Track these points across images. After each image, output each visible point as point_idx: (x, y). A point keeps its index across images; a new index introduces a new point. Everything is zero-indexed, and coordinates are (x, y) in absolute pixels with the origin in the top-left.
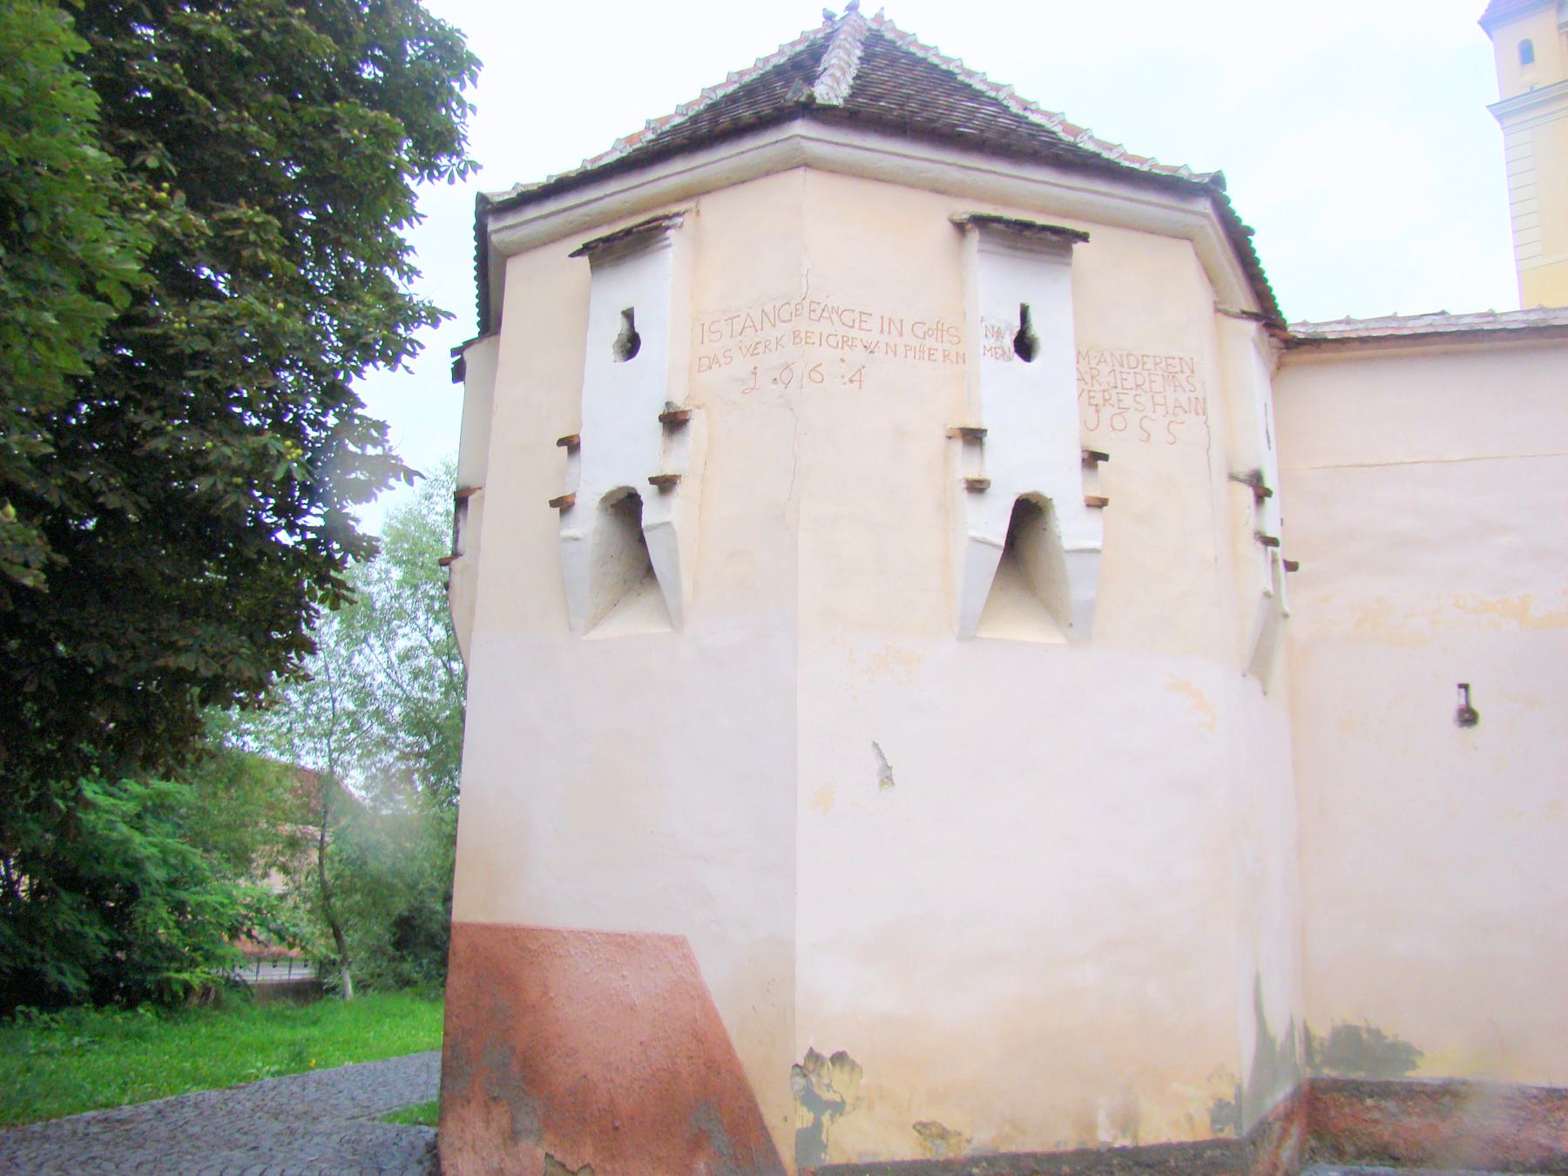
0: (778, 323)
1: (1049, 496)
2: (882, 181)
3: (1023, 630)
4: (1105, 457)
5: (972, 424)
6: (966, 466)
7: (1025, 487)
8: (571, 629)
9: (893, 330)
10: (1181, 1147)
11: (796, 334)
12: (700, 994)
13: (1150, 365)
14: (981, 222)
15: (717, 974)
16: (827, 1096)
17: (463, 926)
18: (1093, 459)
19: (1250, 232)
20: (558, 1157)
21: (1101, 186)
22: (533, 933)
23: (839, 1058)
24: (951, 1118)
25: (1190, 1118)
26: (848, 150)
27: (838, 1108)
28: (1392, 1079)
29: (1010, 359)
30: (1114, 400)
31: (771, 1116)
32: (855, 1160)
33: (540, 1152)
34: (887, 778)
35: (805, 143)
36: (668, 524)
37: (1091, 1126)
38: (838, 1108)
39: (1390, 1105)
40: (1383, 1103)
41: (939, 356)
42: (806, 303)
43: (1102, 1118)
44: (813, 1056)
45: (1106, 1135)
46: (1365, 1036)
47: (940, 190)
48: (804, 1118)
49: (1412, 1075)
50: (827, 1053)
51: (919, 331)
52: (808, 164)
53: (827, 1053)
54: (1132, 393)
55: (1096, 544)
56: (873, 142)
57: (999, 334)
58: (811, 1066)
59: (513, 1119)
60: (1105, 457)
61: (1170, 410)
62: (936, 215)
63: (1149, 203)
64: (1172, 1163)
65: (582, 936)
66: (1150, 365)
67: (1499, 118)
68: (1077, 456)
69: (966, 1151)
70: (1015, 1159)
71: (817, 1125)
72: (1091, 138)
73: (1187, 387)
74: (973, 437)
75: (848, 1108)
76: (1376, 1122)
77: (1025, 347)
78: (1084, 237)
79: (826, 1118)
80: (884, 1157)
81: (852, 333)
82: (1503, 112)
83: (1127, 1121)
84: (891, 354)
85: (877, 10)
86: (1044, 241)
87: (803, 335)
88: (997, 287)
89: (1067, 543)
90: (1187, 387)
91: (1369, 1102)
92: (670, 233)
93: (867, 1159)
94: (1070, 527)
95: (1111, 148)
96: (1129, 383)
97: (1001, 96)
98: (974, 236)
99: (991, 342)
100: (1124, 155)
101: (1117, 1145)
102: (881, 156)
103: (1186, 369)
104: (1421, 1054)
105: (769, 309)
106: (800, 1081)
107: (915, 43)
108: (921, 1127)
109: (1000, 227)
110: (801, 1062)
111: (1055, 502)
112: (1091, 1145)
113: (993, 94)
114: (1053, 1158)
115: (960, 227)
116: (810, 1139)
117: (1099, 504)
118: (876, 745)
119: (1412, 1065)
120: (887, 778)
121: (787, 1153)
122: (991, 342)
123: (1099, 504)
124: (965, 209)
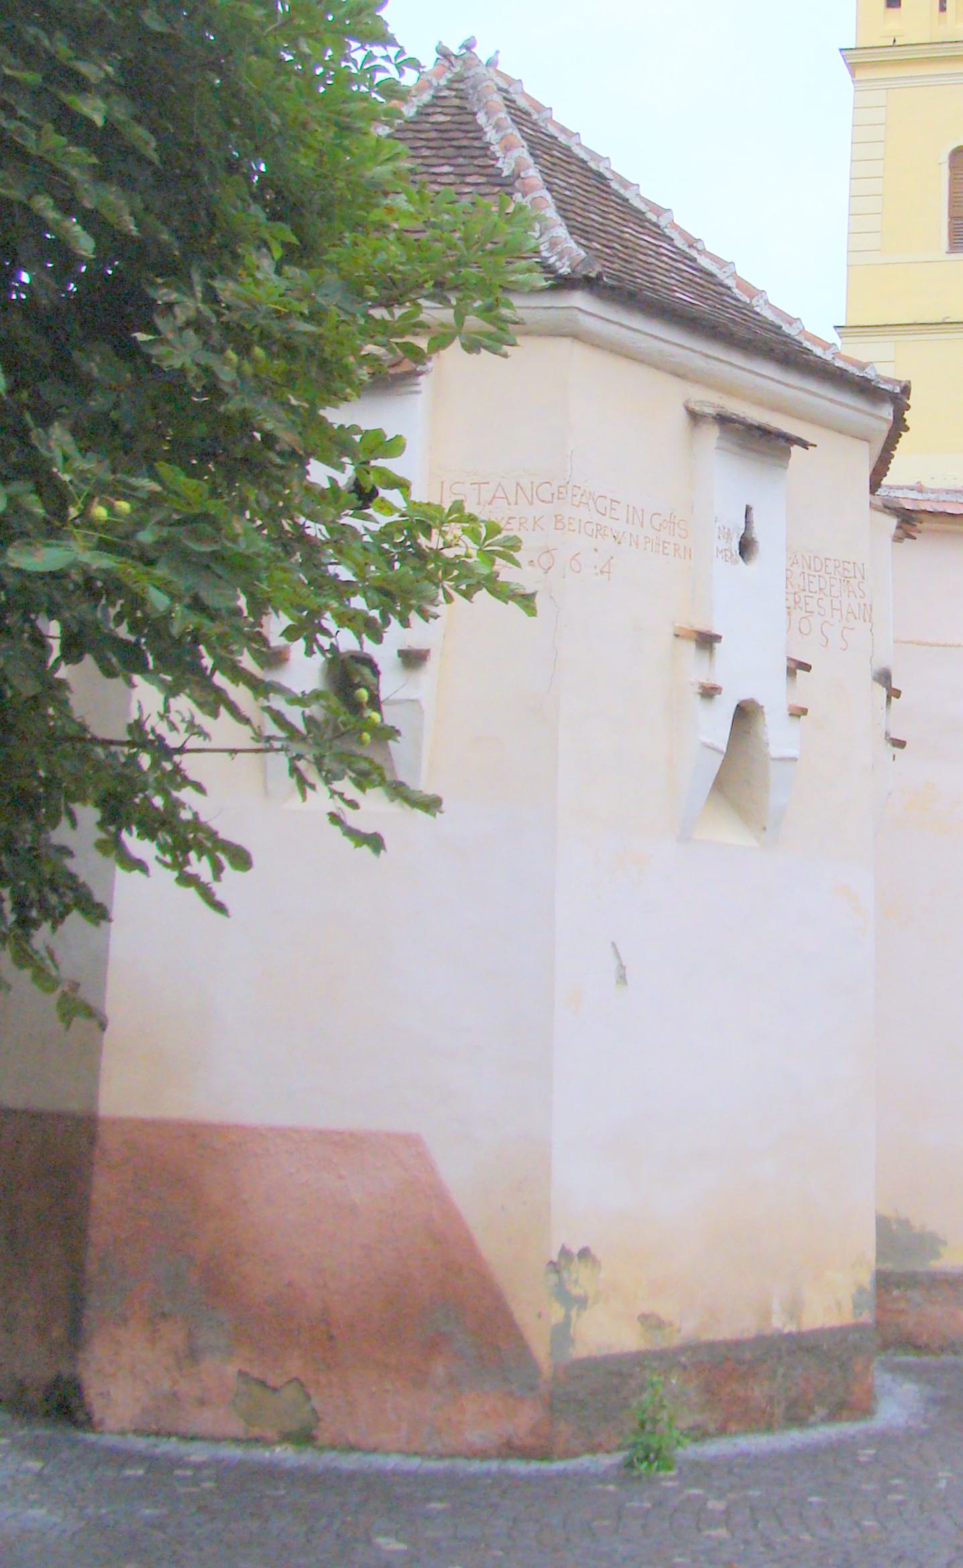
0: (536, 501)
1: (761, 703)
2: (642, 361)
3: (727, 833)
4: (807, 667)
5: (701, 626)
6: (696, 669)
7: (744, 695)
8: (267, 792)
9: (636, 521)
10: (832, 1331)
11: (558, 519)
12: (438, 1194)
13: (831, 569)
14: (724, 420)
15: (460, 1173)
16: (576, 1291)
17: (116, 1122)
18: (797, 667)
19: (907, 429)
20: (256, 1373)
21: (812, 385)
22: (220, 1129)
23: (585, 1253)
24: (665, 1309)
25: (839, 1304)
26: (616, 327)
27: (582, 1302)
28: (920, 1269)
29: (736, 562)
30: (802, 604)
31: (523, 1314)
32: (595, 1353)
33: (231, 1370)
34: (622, 978)
35: (582, 317)
36: (415, 701)
37: (767, 1314)
38: (582, 1302)
39: (916, 1295)
40: (909, 1293)
41: (670, 549)
42: (570, 486)
43: (776, 1306)
44: (565, 1253)
45: (780, 1323)
46: (894, 1226)
47: (680, 373)
48: (557, 1313)
49: (936, 1264)
50: (575, 1249)
51: (657, 521)
52: (577, 336)
53: (575, 1249)
54: (817, 596)
55: (794, 752)
56: (637, 322)
57: (729, 536)
58: (563, 1263)
59: (190, 1335)
60: (807, 667)
61: (844, 613)
62: (671, 398)
63: (847, 406)
64: (825, 1347)
65: (282, 1133)
66: (831, 569)
67: (852, 67)
68: (783, 665)
69: (677, 1341)
70: (712, 1346)
71: (568, 1317)
72: (767, 302)
73: (859, 593)
74: (707, 641)
75: (590, 1302)
76: (902, 1311)
77: (746, 547)
78: (805, 445)
79: (574, 1313)
80: (616, 1349)
81: (606, 521)
82: (858, 60)
83: (794, 1308)
84: (634, 546)
85: (491, 54)
86: (765, 442)
87: (566, 521)
88: (727, 483)
89: (774, 751)
90: (859, 593)
91: (896, 1292)
92: (422, 379)
93: (604, 1352)
94: (778, 735)
95: (791, 321)
96: (815, 587)
97: (663, 222)
98: (711, 435)
99: (722, 544)
100: (802, 331)
101: (786, 1330)
102: (642, 336)
103: (858, 575)
104: (944, 1243)
105: (525, 483)
106: (553, 1278)
107: (550, 119)
108: (644, 1318)
109: (741, 427)
110: (555, 1258)
111: (765, 709)
112: (767, 1332)
113: (654, 218)
114: (737, 1344)
115: (695, 417)
116: (562, 1334)
117: (798, 712)
118: (613, 944)
119: (937, 1255)
120: (622, 978)
121: (540, 1348)
122: (722, 544)
123: (798, 712)
124: (709, 400)
